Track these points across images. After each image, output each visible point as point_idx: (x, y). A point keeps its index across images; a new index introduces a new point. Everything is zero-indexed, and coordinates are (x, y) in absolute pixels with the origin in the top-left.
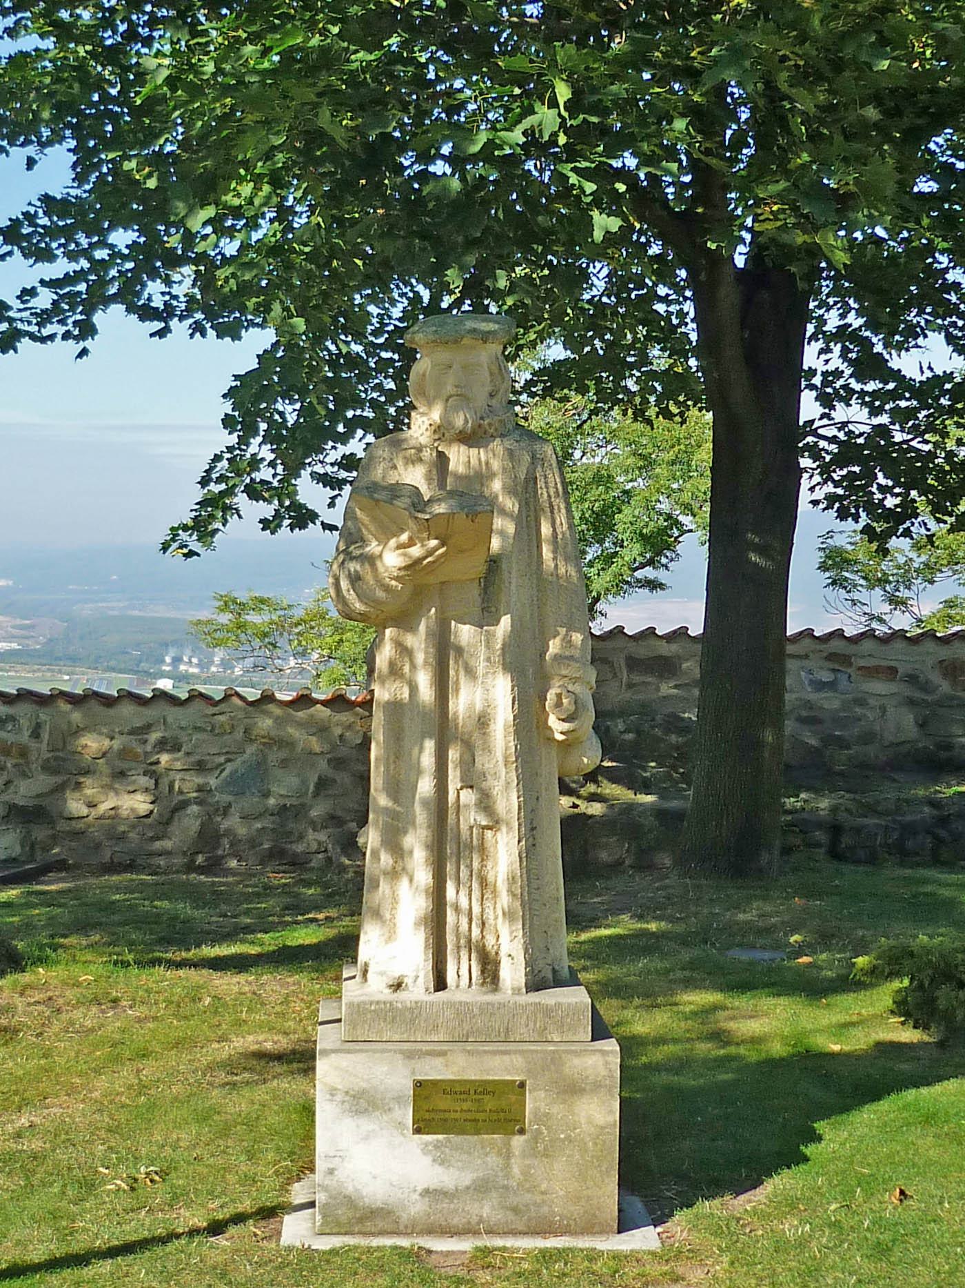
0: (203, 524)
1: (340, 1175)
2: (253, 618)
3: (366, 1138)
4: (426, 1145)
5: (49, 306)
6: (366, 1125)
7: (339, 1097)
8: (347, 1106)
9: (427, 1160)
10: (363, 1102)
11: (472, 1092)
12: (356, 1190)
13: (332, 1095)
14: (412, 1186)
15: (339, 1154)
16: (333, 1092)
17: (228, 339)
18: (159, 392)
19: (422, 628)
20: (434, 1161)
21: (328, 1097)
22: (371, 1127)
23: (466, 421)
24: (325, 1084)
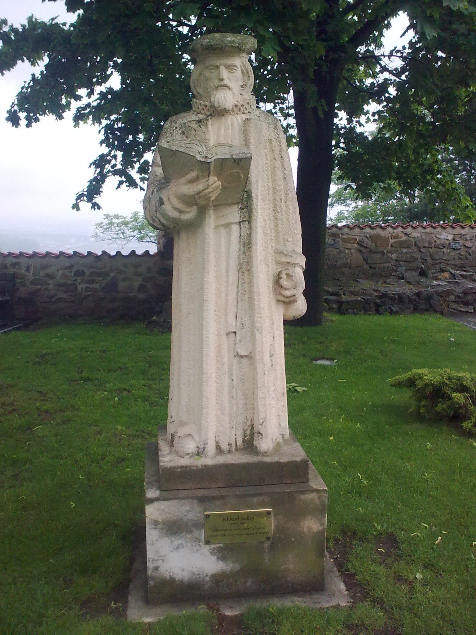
0: (94, 190)
1: (162, 570)
2: (115, 220)
3: (178, 548)
4: (214, 549)
5: (63, 114)
6: (177, 541)
7: (159, 526)
8: (165, 531)
9: (214, 558)
10: (174, 528)
11: (240, 519)
12: (171, 576)
13: (155, 525)
14: (205, 573)
15: (161, 558)
16: (155, 523)
17: (7, 115)
18: (72, 142)
19: (77, 13)
20: (218, 558)
21: (153, 526)
22: (180, 541)
23: (140, 139)
24: (151, 519)
